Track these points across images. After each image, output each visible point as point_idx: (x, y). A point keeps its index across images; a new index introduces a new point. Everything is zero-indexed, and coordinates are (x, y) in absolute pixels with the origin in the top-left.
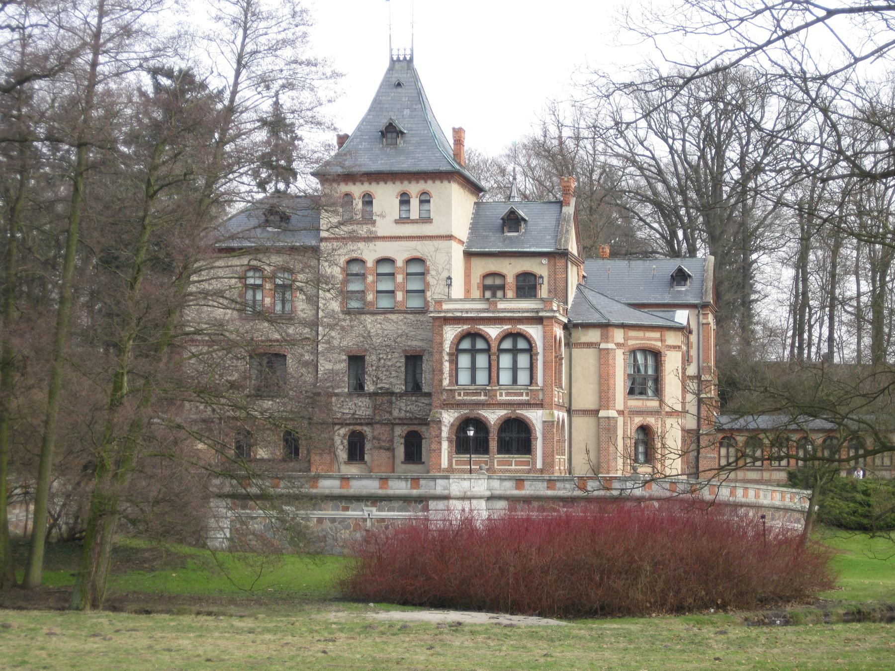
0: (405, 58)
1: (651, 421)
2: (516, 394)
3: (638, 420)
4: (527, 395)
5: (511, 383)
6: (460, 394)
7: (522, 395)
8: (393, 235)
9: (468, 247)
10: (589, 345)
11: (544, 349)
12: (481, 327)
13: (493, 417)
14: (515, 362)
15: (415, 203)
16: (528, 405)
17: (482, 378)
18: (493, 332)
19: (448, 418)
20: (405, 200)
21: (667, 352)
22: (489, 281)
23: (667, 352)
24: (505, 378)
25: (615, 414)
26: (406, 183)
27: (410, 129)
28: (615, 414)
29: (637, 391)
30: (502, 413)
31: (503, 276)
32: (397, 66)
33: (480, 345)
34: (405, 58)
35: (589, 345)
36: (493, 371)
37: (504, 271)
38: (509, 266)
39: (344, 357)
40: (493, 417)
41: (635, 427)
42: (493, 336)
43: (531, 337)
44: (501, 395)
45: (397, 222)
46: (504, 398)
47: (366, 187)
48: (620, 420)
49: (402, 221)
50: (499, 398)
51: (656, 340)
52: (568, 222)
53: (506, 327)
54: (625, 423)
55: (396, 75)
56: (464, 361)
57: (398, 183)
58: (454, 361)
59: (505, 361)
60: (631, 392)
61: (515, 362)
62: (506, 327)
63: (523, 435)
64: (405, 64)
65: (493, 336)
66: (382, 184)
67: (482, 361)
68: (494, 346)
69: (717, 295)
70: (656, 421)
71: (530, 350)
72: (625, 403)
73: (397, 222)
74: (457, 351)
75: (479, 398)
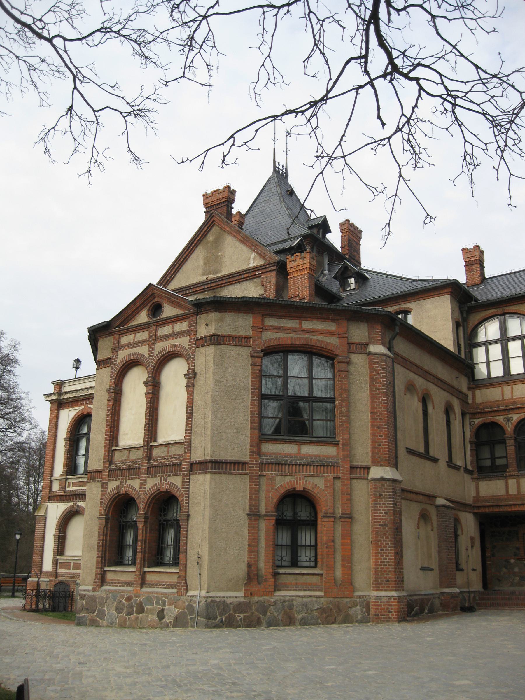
1: (316, 484)
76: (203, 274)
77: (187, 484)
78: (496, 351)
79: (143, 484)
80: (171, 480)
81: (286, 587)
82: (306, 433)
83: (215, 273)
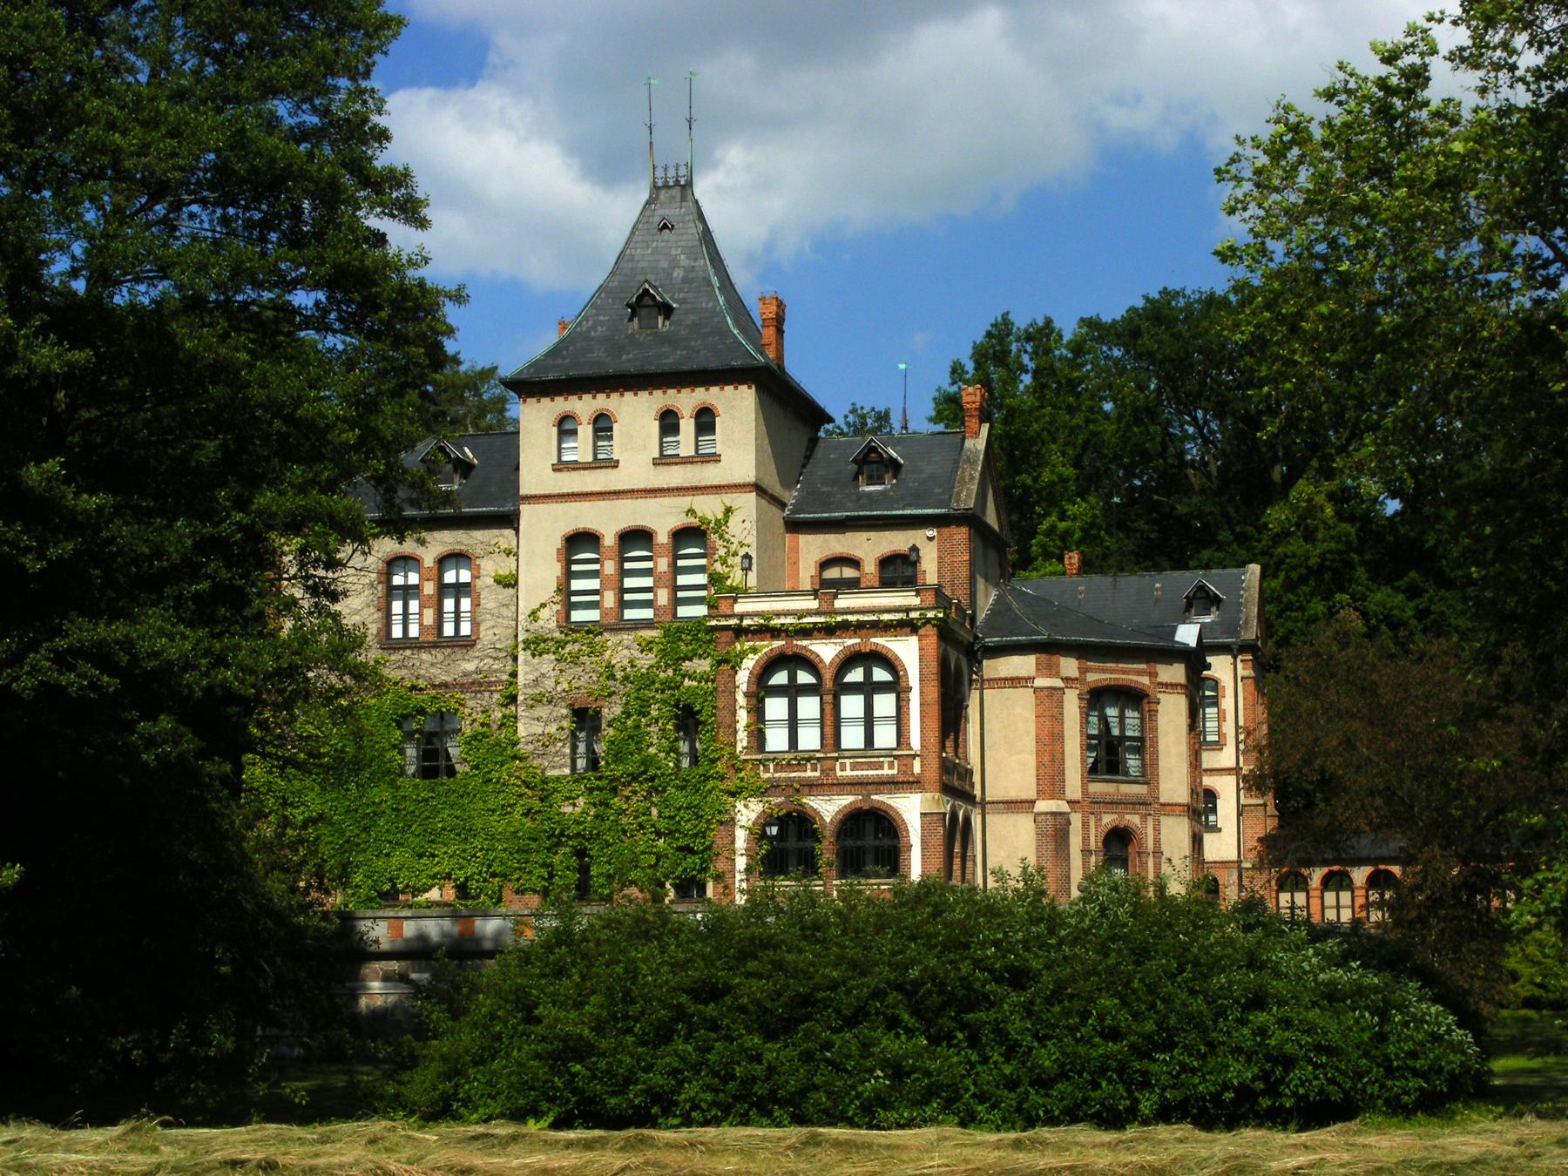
0: (677, 182)
1: (1134, 820)
2: (871, 766)
3: (1108, 820)
4: (891, 766)
5: (862, 746)
6: (767, 770)
7: (882, 768)
8: (650, 486)
9: (793, 512)
10: (1015, 682)
11: (921, 681)
12: (804, 643)
13: (828, 808)
14: (869, 707)
15: (687, 426)
16: (893, 785)
17: (809, 739)
18: (827, 651)
19: (748, 812)
20: (668, 422)
21: (1160, 696)
22: (832, 573)
23: (1160, 696)
24: (852, 737)
25: (1065, 807)
26: (672, 392)
27: (682, 302)
28: (1065, 807)
29: (908, 572)
30: (845, 801)
31: (854, 563)
32: (663, 195)
33: (804, 678)
34: (677, 182)
35: (1015, 682)
36: (832, 723)
37: (857, 553)
38: (866, 544)
39: (564, 711)
40: (828, 808)
41: (1103, 830)
42: (827, 661)
43: (897, 658)
44: (843, 769)
45: (656, 463)
46: (848, 773)
47: (601, 402)
48: (1076, 820)
49: (663, 460)
50: (839, 773)
51: (1139, 673)
52: (972, 463)
53: (850, 642)
54: (1085, 825)
55: (661, 212)
56: (776, 708)
57: (658, 393)
58: (758, 712)
59: (852, 705)
60: (1093, 771)
61: (869, 707)
62: (850, 642)
63: (887, 842)
64: (676, 192)
65: (827, 661)
66: (629, 395)
67: (809, 707)
68: (828, 676)
69: (1266, 625)
70: (1144, 818)
71: (897, 686)
72: (1085, 792)
73: (656, 463)
74: (761, 689)
75: (803, 774)
80: (1128, 817)
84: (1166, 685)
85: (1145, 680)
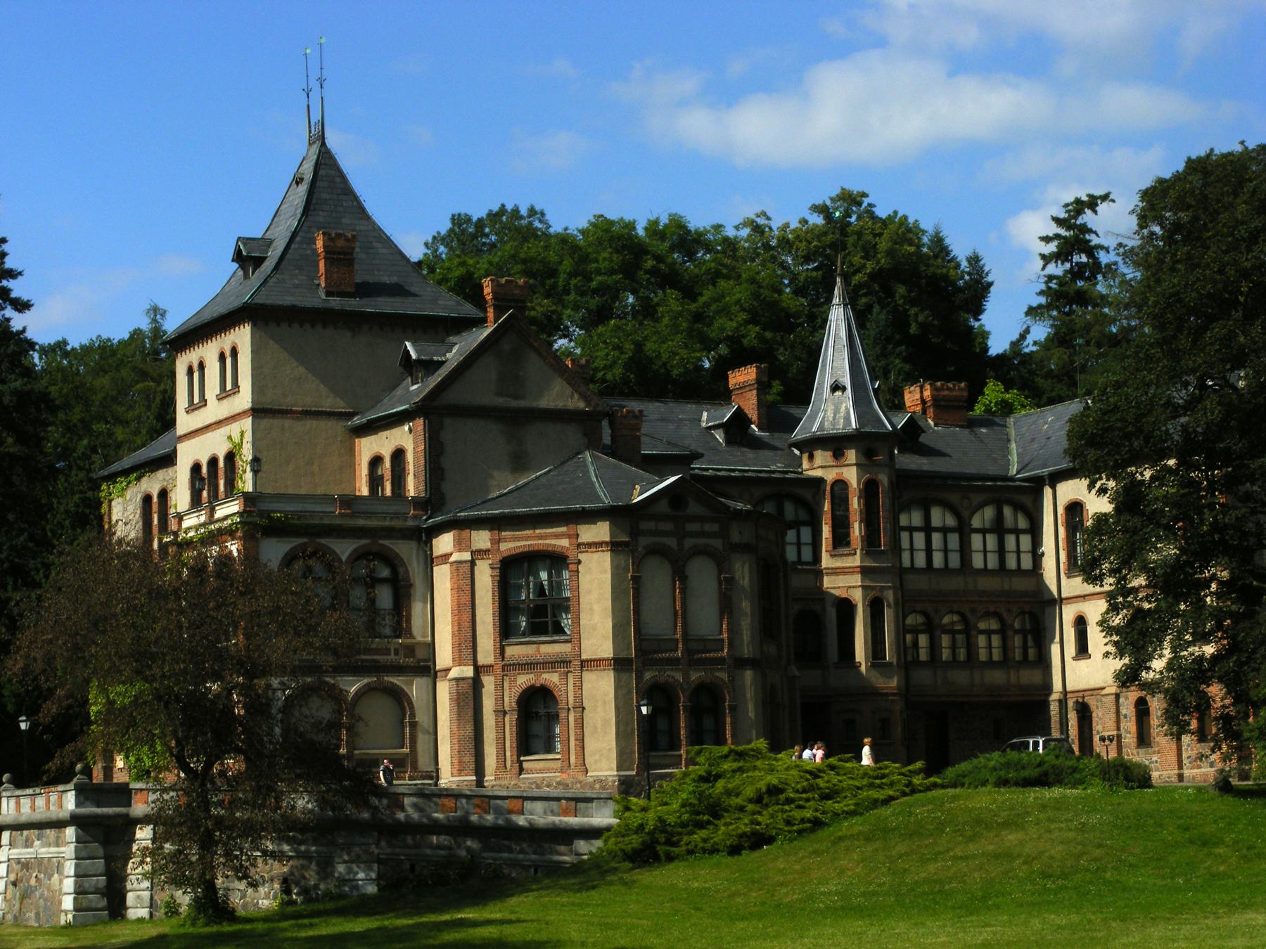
1: (551, 678)
3: (524, 680)
54: (500, 688)
76: (499, 394)
77: (732, 679)
78: (919, 538)
79: (686, 676)
80: (545, 676)
81: (531, 771)
82: (835, 547)
83: (516, 397)
84: (590, 545)
85: (565, 543)
